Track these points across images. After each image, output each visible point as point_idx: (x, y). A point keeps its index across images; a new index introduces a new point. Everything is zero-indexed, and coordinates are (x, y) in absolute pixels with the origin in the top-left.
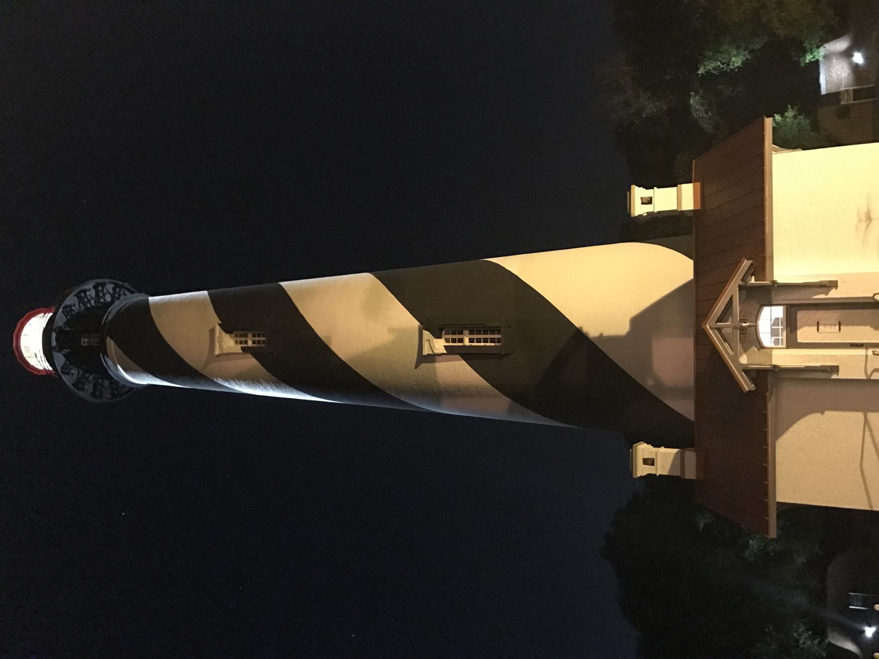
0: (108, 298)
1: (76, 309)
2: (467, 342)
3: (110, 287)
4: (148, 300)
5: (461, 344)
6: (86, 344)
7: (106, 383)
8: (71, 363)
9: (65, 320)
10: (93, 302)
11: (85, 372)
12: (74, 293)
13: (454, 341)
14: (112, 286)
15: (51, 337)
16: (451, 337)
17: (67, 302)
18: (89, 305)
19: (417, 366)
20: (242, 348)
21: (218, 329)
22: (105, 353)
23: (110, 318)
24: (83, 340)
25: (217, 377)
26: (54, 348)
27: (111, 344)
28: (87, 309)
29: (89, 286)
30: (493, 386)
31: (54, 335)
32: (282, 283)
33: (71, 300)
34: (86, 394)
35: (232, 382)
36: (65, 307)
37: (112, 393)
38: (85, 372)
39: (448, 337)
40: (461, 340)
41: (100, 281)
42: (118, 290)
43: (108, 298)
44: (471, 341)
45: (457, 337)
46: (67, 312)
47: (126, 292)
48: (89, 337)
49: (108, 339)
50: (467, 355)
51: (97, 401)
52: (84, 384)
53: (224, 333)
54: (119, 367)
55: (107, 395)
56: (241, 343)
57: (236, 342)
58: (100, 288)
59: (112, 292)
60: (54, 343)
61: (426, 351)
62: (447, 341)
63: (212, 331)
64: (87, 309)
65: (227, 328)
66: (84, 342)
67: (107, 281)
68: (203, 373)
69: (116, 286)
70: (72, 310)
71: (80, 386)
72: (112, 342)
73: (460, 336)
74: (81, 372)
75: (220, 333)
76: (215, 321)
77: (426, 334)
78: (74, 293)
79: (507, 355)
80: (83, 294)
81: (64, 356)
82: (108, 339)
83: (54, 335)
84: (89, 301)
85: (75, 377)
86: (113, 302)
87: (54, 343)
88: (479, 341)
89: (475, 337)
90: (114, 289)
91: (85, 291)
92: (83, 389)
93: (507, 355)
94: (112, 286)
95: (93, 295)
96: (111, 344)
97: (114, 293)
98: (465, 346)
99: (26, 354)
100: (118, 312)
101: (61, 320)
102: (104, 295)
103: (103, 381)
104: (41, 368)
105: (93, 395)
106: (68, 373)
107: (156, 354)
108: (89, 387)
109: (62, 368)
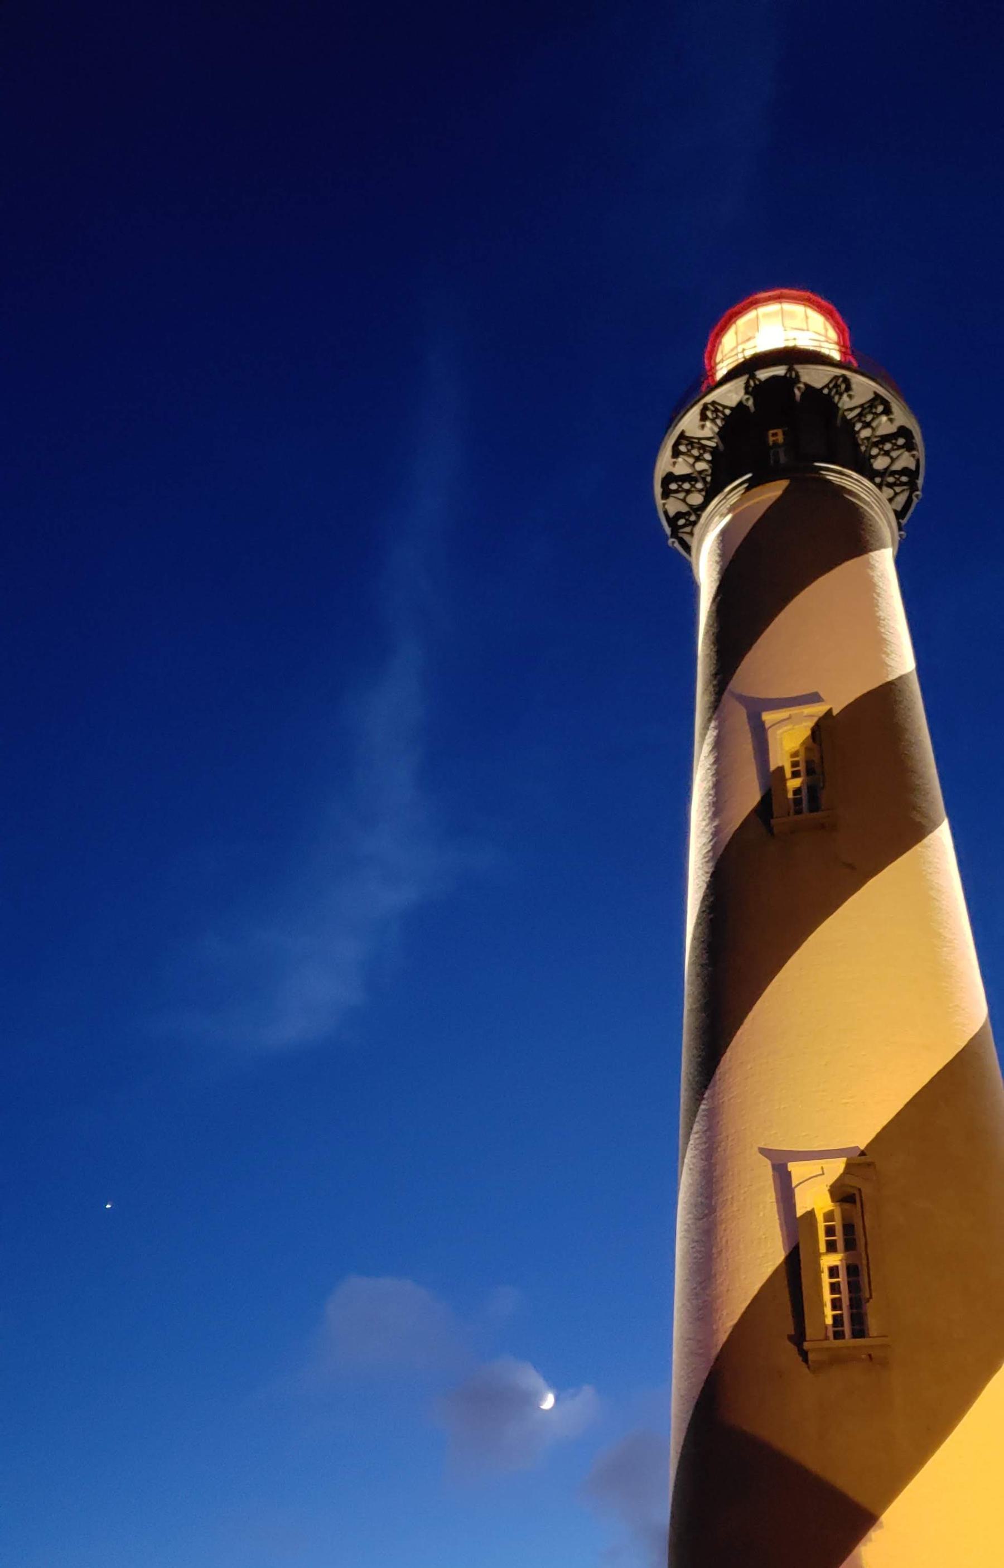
0: (880, 463)
1: (845, 402)
2: (830, 1260)
3: (905, 460)
4: (883, 546)
5: (823, 1248)
6: (771, 439)
7: (696, 499)
8: (726, 418)
9: (818, 385)
10: (866, 433)
11: (714, 452)
12: (882, 391)
13: (830, 1231)
14: (913, 467)
15: (774, 364)
16: (838, 1224)
17: (858, 380)
18: (858, 426)
19: (765, 1152)
20: (781, 769)
21: (819, 710)
22: (752, 484)
23: (831, 477)
24: (780, 432)
25: (719, 728)
26: (752, 376)
27: (773, 491)
28: (851, 424)
29: (902, 416)
30: (737, 1327)
31: (780, 371)
32: (942, 838)
33: (864, 386)
34: (665, 463)
35: (711, 759)
36: (846, 380)
37: (679, 515)
38: (714, 452)
39: (838, 1216)
40: (831, 1247)
41: (918, 438)
42: (904, 479)
43: (880, 463)
44: (833, 1271)
45: (839, 1237)
46: (836, 386)
47: (902, 499)
48: (785, 444)
49: (784, 484)
50: (794, 1268)
51: (658, 490)
52: (688, 454)
53: (811, 724)
54: (729, 517)
55: (674, 506)
56: (795, 764)
57: (795, 754)
58: (901, 441)
59: (897, 466)
60: (763, 375)
61: (797, 1170)
62: (829, 1216)
63: (814, 698)
64: (851, 424)
65: (822, 731)
66: (777, 436)
67: (921, 452)
68: (726, 694)
69: (912, 474)
70: (841, 395)
71: (683, 448)
72: (779, 493)
73: (840, 1245)
74: (712, 444)
75: (812, 716)
76: (837, 701)
77: (837, 1167)
78: (882, 391)
79: (804, 1355)
80: (880, 408)
81: (740, 404)
82: (784, 484)
83: (780, 371)
84: (867, 425)
85: (700, 434)
86: (870, 474)
87: (763, 375)
88: (834, 1288)
89: (842, 1279)
90: (905, 471)
91: (887, 411)
92: (676, 453)
93: (804, 1355)
94: (913, 467)
95: (882, 431)
96: (773, 491)
97: (893, 473)
98: (818, 1255)
99: (742, 322)
100: (843, 489)
101: (815, 377)
102: (887, 453)
103: (700, 491)
104: (719, 357)
105: (669, 478)
106: (703, 417)
107: (760, 584)
108: (682, 468)
109: (714, 403)
